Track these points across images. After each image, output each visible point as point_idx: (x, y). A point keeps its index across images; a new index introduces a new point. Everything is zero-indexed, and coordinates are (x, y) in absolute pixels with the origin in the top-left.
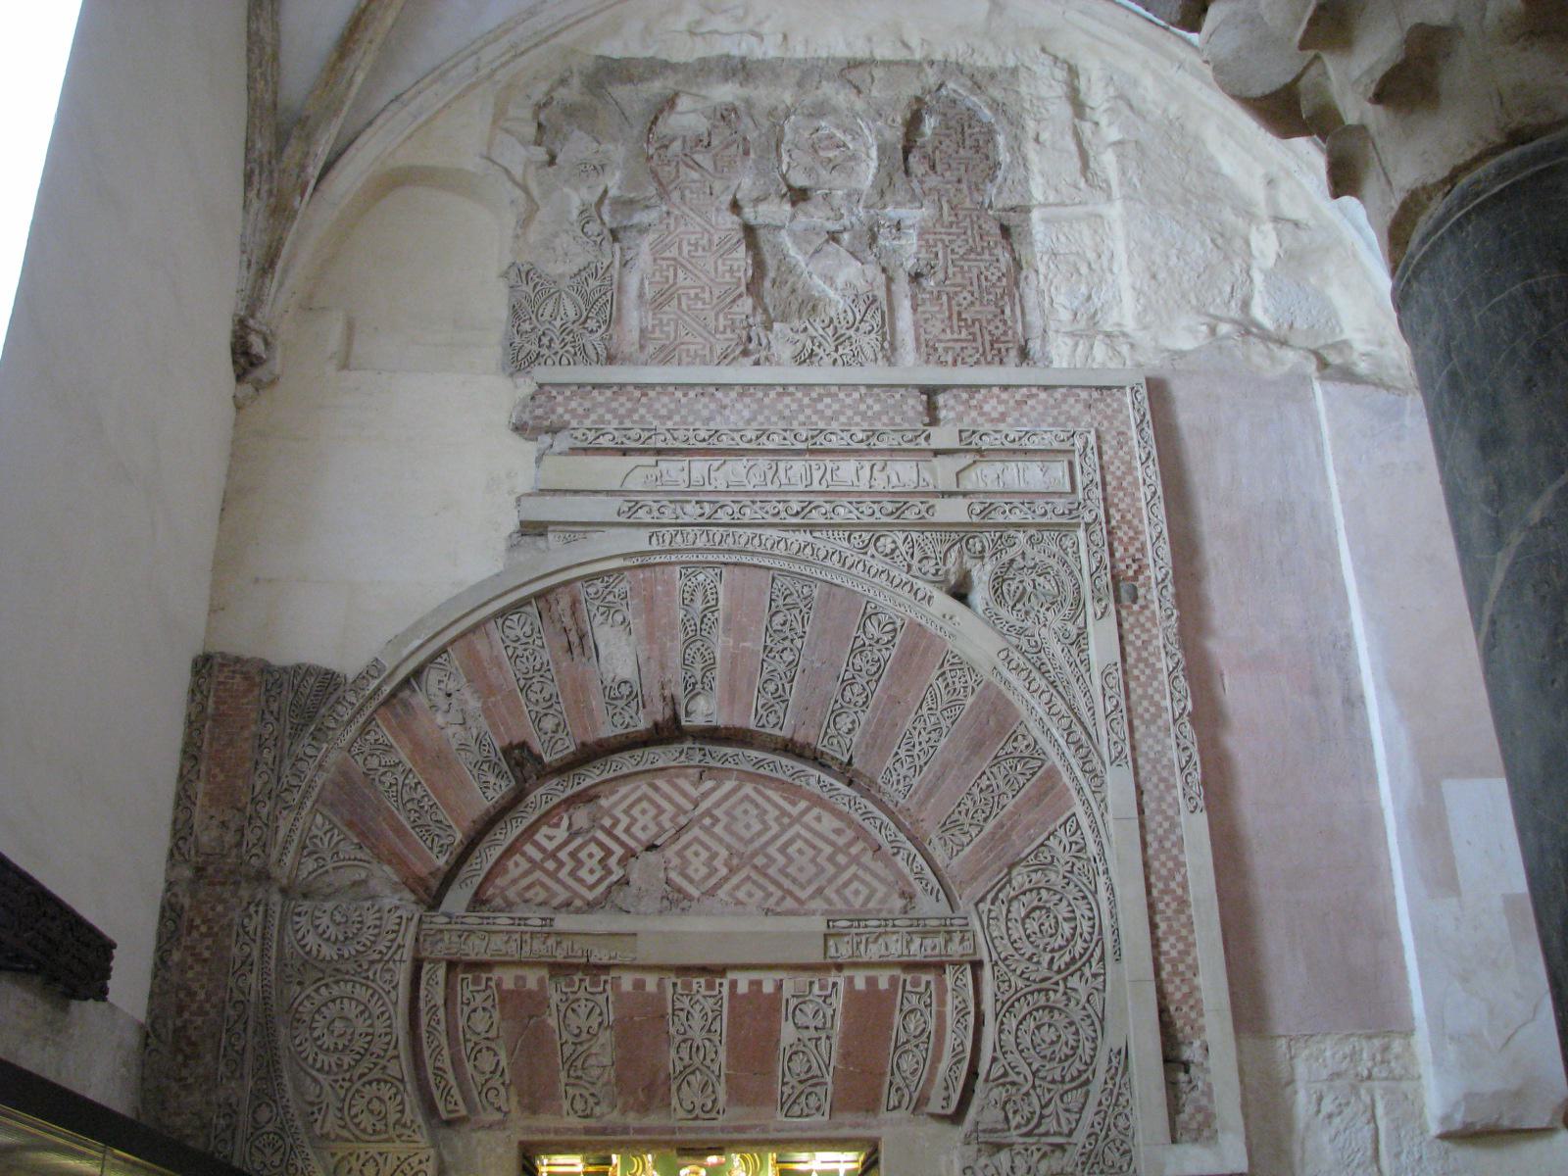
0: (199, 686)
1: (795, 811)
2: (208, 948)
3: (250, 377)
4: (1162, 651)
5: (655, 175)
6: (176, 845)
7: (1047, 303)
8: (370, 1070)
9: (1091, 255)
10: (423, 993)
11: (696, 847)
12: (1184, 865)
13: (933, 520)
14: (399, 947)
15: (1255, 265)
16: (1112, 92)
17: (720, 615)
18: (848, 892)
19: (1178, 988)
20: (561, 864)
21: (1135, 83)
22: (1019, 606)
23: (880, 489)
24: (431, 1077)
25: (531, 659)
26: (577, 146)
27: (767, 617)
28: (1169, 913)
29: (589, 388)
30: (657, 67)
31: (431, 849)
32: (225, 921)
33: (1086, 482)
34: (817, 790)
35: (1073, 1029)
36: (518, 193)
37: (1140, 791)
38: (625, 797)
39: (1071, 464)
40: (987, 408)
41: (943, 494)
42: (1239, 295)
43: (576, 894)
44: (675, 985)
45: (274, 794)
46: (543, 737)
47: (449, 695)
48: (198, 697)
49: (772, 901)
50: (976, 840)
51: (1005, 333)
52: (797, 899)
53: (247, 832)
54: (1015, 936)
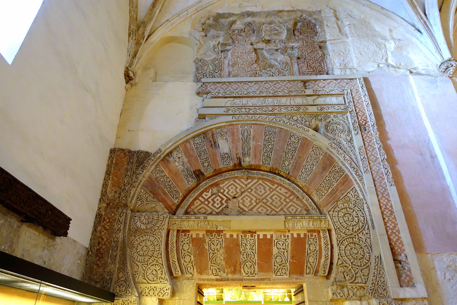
0: (111, 156)
1: (274, 187)
2: (108, 226)
3: (130, 83)
4: (375, 143)
5: (231, 37)
6: (102, 198)
7: (333, 62)
8: (153, 261)
9: (344, 51)
10: (170, 239)
11: (246, 197)
12: (391, 201)
13: (308, 111)
14: (163, 225)
15: (388, 50)
16: (346, 14)
17: (252, 136)
18: (290, 209)
19: (394, 238)
20: (209, 202)
21: (352, 11)
22: (333, 133)
23: (293, 104)
24: (171, 264)
25: (201, 148)
26: (213, 32)
27: (264, 137)
28: (388, 215)
29: (216, 83)
30: (231, 15)
31: (173, 198)
32: (114, 218)
33: (349, 101)
34: (280, 182)
35: (362, 249)
36: (197, 42)
37: (374, 181)
38: (227, 184)
39: (344, 98)
40: (320, 85)
41: (310, 105)
42: (384, 58)
43: (214, 210)
44: (242, 236)
45: (130, 183)
46: (204, 168)
47: (179, 158)
48: (111, 158)
49: (269, 212)
50: (326, 194)
51: (322, 70)
52: (276, 211)
53: (122, 193)
54: (341, 221)
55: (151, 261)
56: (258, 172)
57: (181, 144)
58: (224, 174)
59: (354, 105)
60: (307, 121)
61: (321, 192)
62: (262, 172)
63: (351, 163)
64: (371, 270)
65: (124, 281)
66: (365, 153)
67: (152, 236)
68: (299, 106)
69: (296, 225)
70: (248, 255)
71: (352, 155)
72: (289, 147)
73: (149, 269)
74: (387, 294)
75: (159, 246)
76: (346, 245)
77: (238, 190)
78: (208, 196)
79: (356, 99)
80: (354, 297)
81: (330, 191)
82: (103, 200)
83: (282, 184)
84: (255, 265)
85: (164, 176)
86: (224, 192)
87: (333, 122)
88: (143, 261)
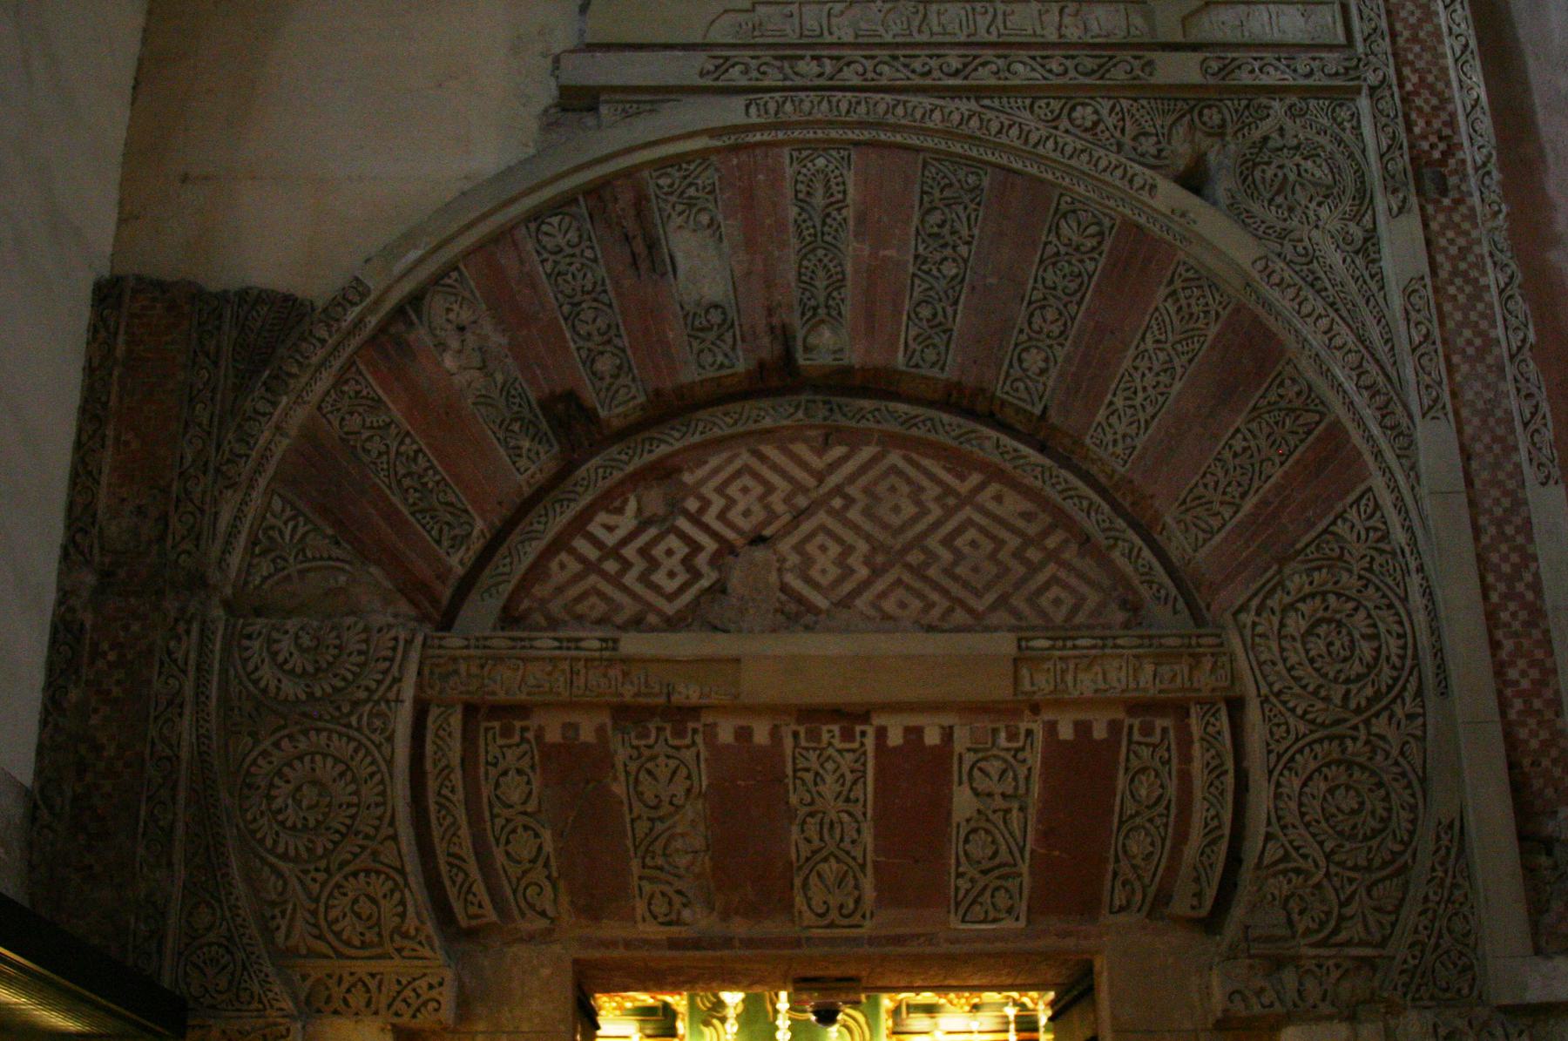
1: (964, 488)
2: (118, 682)
4: (1489, 261)
8: (356, 855)
10: (429, 748)
11: (820, 538)
13: (1152, 80)
17: (849, 213)
18: (1044, 601)
20: (626, 565)
22: (1279, 200)
23: (1074, 39)
24: (444, 868)
31: (438, 542)
34: (995, 458)
35: (1382, 792)
38: (715, 471)
43: (650, 607)
44: (796, 735)
45: (211, 466)
47: (462, 329)
48: (103, 334)
49: (936, 613)
50: (1229, 526)
52: (971, 611)
54: (1293, 659)
56: (882, 404)
57: (467, 254)
58: (701, 414)
59: (1395, 55)
60: (1146, 134)
62: (903, 408)
63: (1360, 365)
65: (220, 945)
66: (1434, 311)
67: (340, 735)
68: (1106, 50)
69: (1069, 678)
71: (1370, 321)
72: (1049, 275)
73: (336, 893)
74: (1471, 988)
75: (382, 782)
76: (1308, 772)
77: (776, 501)
78: (621, 533)
79: (1405, 20)
80: (1325, 1008)
81: (1248, 505)
82: (82, 553)
83: (1008, 467)
85: (389, 425)
86: (702, 510)
87: (1280, 143)
88: (305, 855)
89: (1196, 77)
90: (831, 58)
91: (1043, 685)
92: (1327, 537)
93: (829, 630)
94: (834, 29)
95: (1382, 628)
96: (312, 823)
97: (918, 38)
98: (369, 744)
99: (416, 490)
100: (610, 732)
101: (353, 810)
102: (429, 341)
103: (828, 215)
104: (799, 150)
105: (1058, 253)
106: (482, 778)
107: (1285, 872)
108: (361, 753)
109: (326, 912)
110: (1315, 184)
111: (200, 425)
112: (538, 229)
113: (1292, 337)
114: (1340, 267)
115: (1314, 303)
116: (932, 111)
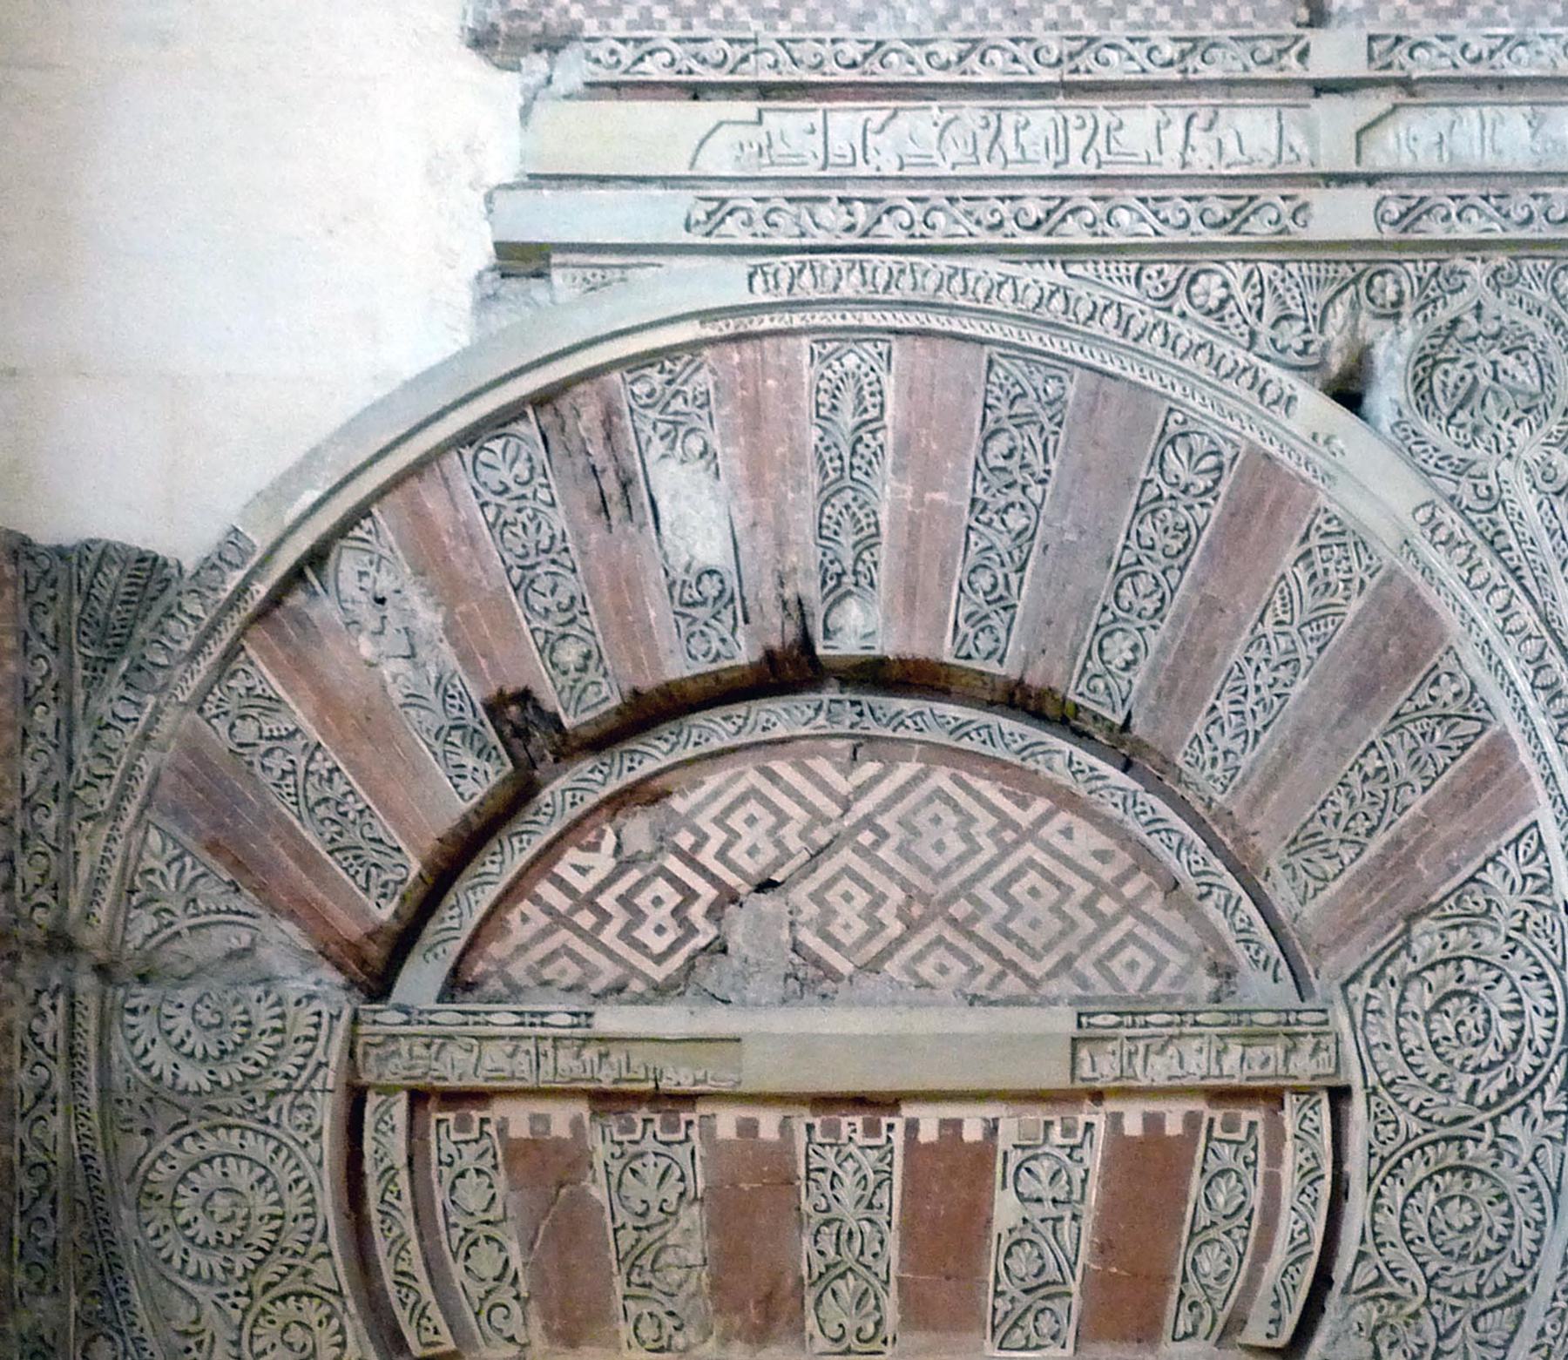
1: (1024, 818)
10: (368, 1146)
11: (846, 884)
14: (320, 1065)
17: (888, 438)
18: (1116, 966)
20: (604, 917)
22: (1462, 416)
24: (391, 1289)
25: (532, 527)
31: (366, 890)
34: (1065, 778)
35: (1504, 1206)
38: (716, 794)
44: (810, 1127)
46: (561, 680)
47: (382, 601)
49: (983, 979)
50: (1351, 870)
52: (1025, 977)
53: (21, 861)
54: (1411, 1044)
55: (266, 1276)
61: (1316, 856)
64: (1526, 1321)
69: (1138, 1061)
70: (844, 1237)
73: (261, 1321)
75: (310, 1188)
76: (1415, 1180)
81: (1375, 846)
83: (1082, 791)
84: (881, 1292)
85: (292, 735)
86: (697, 846)
89: (1366, 230)
90: (864, 200)
91: (1106, 1070)
92: (1473, 886)
93: (849, 1003)
94: (871, 153)
95: (1528, 1005)
96: (227, 1239)
97: (986, 169)
98: (292, 1144)
99: (334, 822)
100: (587, 1123)
101: (277, 1223)
102: (337, 617)
103: (860, 439)
104: (823, 342)
105: (1160, 497)
106: (435, 1180)
107: (1375, 1298)
108: (284, 1154)
109: (251, 1343)
110: (1513, 392)
111: (43, 735)
112: (475, 457)
113: (1456, 618)
114: (1532, 515)
115: (1492, 569)
116: (1000, 285)
